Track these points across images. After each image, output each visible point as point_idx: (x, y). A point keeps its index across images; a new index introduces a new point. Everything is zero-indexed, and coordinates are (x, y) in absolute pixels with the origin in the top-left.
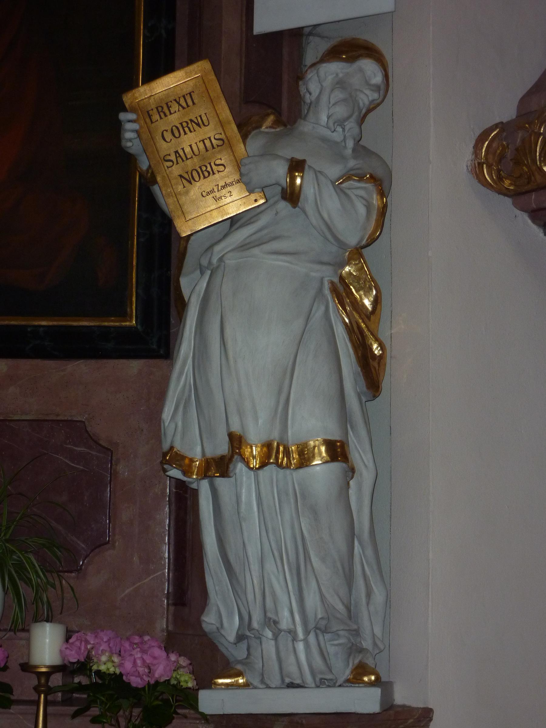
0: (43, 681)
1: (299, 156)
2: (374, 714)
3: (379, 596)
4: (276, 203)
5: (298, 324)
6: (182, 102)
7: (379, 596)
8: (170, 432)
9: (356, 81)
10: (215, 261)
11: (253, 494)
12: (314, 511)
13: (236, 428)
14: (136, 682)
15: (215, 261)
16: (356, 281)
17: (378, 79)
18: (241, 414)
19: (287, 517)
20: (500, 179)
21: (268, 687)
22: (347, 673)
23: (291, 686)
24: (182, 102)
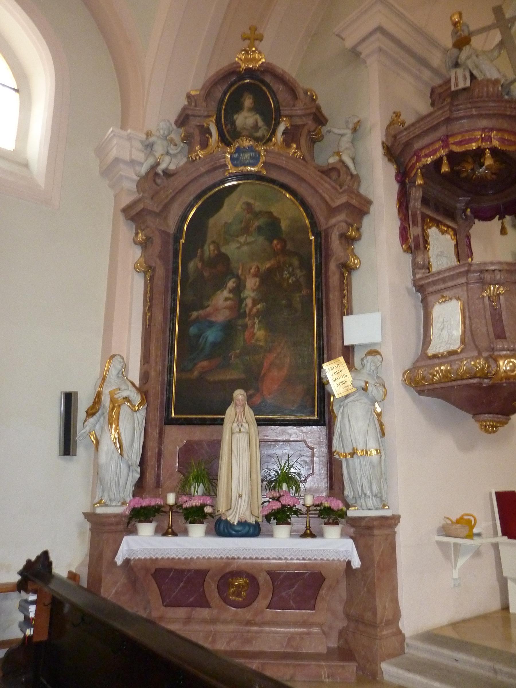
0: (308, 508)
1: (367, 380)
2: (37, 596)
3: (386, 487)
4: (360, 390)
5: (368, 421)
6: (337, 367)
7: (386, 487)
8: (335, 447)
9: (376, 360)
10: (345, 404)
11: (226, 435)
12: (374, 466)
13: (355, 446)
14: (335, 509)
15: (345, 404)
16: (310, 361)
17: (381, 360)
18: (356, 442)
19: (367, 468)
20: (410, 383)
21: (363, 509)
22: (381, 506)
23: (370, 509)
24: (337, 367)
